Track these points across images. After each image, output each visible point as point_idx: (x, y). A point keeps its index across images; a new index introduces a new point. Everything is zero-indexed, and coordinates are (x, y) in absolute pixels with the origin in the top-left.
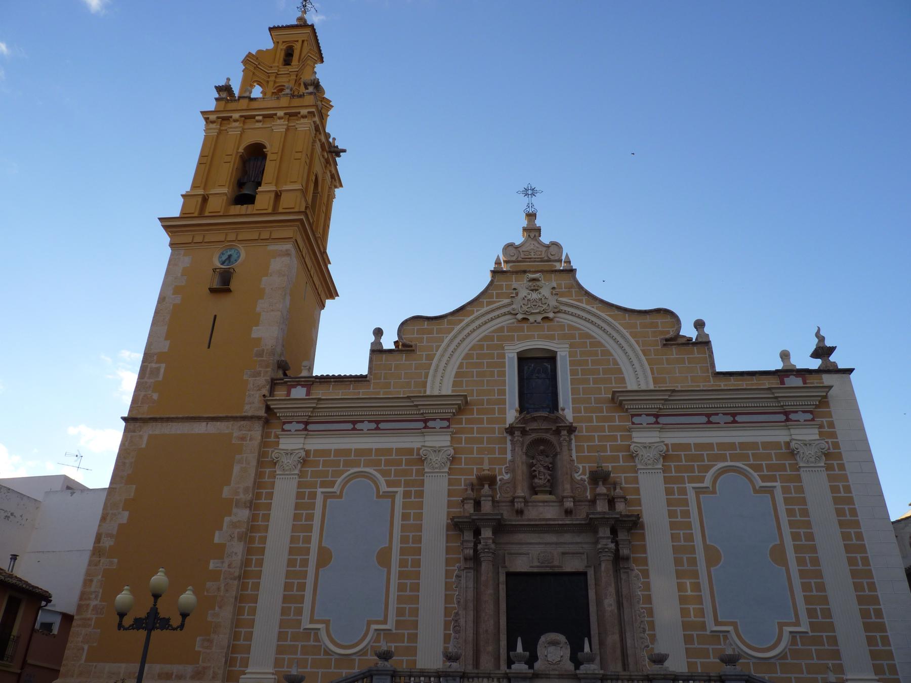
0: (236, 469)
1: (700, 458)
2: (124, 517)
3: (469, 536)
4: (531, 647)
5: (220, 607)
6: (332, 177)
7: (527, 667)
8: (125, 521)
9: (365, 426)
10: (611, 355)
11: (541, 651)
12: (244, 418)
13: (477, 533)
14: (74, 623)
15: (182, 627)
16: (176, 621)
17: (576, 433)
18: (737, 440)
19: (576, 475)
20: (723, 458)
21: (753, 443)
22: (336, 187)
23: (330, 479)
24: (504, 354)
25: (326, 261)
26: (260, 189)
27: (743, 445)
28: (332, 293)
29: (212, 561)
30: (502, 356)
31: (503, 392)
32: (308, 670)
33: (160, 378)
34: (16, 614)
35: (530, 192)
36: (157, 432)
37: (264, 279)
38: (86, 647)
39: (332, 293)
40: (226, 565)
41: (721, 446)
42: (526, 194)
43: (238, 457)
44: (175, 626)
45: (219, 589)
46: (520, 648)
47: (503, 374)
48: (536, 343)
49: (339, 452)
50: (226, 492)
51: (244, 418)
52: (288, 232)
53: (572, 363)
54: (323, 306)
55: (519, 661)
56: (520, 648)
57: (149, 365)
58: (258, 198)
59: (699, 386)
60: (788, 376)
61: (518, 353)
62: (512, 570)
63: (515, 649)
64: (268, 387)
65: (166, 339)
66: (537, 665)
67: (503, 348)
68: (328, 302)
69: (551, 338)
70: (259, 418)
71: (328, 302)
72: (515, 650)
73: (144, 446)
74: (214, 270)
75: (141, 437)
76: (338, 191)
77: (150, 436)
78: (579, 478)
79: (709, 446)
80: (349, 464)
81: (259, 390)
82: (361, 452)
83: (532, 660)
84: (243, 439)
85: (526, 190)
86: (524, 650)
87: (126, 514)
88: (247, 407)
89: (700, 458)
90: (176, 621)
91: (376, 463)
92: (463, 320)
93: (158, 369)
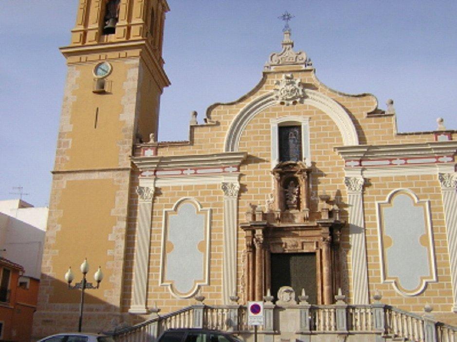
0: (117, 199)
1: (384, 186)
2: (59, 227)
3: (249, 233)
4: (274, 293)
5: (115, 275)
6: (163, 6)
7: (307, 303)
8: (59, 229)
9: (189, 172)
10: (334, 123)
11: (279, 295)
12: (119, 170)
13: (254, 232)
14: (41, 284)
15: (98, 287)
16: (95, 285)
17: (312, 172)
18: (406, 175)
19: (311, 197)
20: (397, 185)
21: (416, 176)
22: (166, 12)
23: (169, 203)
24: (270, 126)
25: (161, 62)
26: (117, 24)
27: (410, 177)
28: (167, 83)
29: (108, 250)
30: (269, 126)
31: (269, 149)
32: (164, 306)
33: (70, 147)
34: (8, 278)
35: (287, 17)
36: (71, 179)
37: (125, 83)
38: (48, 295)
39: (167, 83)
40: (116, 252)
41: (397, 178)
42: (284, 19)
43: (118, 192)
44: (94, 287)
45: (113, 265)
46: (303, 294)
47: (269, 138)
48: (290, 118)
49: (174, 188)
50: (113, 212)
51: (119, 170)
52: (137, 52)
53: (311, 130)
54: (161, 92)
55: (268, 300)
56: (303, 294)
57: (63, 140)
58: (117, 30)
59: (386, 142)
60: (440, 135)
61: (279, 124)
62: (274, 252)
63: (301, 294)
64: (131, 150)
65: (71, 123)
66: (278, 303)
67: (269, 122)
68: (165, 89)
69: (299, 114)
70: (128, 169)
71: (165, 89)
72: (301, 295)
73: (64, 187)
74: (94, 80)
75: (62, 182)
76: (167, 14)
77: (68, 182)
78: (313, 199)
79: (390, 178)
80: (180, 194)
81: (126, 152)
82: (186, 188)
83: (275, 300)
84: (119, 181)
85: (284, 16)
86: (306, 294)
87: (60, 226)
88: (120, 163)
89: (384, 186)
90: (95, 285)
91: (196, 194)
92: (245, 104)
93: (68, 142)
